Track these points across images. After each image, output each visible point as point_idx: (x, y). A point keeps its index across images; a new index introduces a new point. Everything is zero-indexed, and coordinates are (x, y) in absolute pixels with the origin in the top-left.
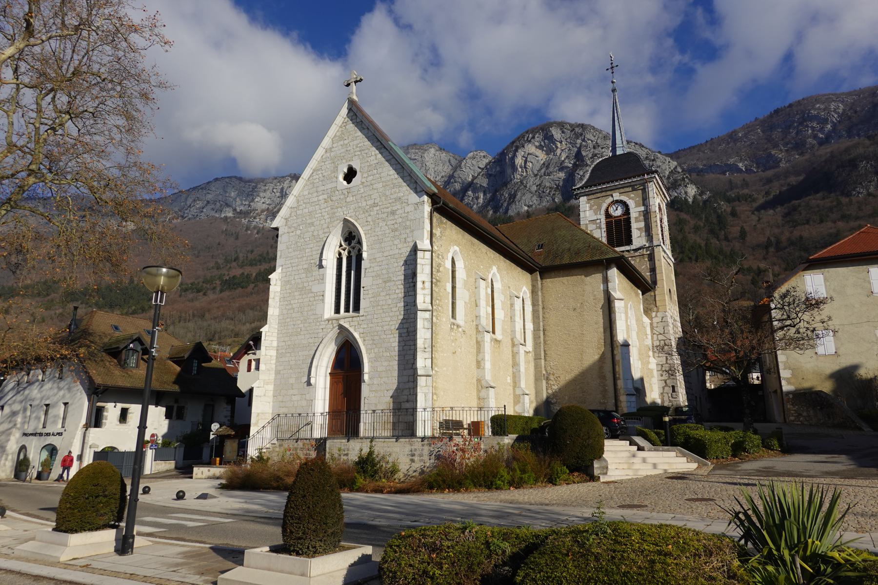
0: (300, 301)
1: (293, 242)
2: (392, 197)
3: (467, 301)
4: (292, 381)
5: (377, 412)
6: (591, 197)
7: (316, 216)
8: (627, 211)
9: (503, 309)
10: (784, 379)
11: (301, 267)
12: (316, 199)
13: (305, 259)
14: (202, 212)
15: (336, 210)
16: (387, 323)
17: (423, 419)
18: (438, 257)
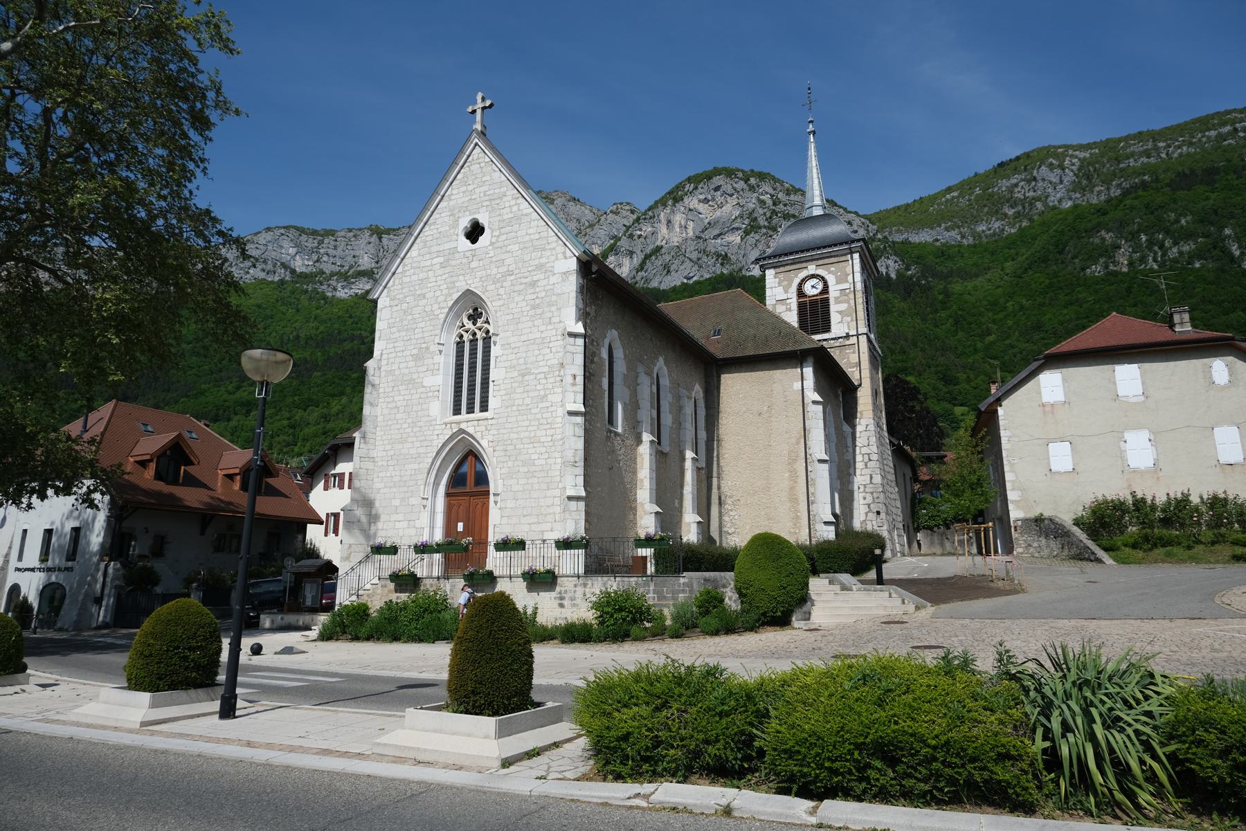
0: (406, 398)
1: (398, 320)
2: (532, 263)
3: (628, 402)
4: (396, 502)
5: (548, 542)
6: (782, 269)
7: (429, 285)
8: (825, 290)
9: (670, 413)
10: (1013, 502)
11: (408, 353)
12: (429, 263)
13: (413, 341)
14: (248, 273)
15: (455, 279)
16: (525, 429)
17: (542, 554)
18: (592, 344)
